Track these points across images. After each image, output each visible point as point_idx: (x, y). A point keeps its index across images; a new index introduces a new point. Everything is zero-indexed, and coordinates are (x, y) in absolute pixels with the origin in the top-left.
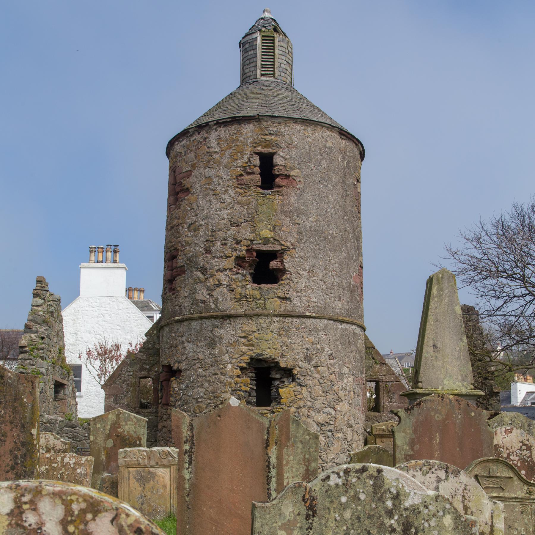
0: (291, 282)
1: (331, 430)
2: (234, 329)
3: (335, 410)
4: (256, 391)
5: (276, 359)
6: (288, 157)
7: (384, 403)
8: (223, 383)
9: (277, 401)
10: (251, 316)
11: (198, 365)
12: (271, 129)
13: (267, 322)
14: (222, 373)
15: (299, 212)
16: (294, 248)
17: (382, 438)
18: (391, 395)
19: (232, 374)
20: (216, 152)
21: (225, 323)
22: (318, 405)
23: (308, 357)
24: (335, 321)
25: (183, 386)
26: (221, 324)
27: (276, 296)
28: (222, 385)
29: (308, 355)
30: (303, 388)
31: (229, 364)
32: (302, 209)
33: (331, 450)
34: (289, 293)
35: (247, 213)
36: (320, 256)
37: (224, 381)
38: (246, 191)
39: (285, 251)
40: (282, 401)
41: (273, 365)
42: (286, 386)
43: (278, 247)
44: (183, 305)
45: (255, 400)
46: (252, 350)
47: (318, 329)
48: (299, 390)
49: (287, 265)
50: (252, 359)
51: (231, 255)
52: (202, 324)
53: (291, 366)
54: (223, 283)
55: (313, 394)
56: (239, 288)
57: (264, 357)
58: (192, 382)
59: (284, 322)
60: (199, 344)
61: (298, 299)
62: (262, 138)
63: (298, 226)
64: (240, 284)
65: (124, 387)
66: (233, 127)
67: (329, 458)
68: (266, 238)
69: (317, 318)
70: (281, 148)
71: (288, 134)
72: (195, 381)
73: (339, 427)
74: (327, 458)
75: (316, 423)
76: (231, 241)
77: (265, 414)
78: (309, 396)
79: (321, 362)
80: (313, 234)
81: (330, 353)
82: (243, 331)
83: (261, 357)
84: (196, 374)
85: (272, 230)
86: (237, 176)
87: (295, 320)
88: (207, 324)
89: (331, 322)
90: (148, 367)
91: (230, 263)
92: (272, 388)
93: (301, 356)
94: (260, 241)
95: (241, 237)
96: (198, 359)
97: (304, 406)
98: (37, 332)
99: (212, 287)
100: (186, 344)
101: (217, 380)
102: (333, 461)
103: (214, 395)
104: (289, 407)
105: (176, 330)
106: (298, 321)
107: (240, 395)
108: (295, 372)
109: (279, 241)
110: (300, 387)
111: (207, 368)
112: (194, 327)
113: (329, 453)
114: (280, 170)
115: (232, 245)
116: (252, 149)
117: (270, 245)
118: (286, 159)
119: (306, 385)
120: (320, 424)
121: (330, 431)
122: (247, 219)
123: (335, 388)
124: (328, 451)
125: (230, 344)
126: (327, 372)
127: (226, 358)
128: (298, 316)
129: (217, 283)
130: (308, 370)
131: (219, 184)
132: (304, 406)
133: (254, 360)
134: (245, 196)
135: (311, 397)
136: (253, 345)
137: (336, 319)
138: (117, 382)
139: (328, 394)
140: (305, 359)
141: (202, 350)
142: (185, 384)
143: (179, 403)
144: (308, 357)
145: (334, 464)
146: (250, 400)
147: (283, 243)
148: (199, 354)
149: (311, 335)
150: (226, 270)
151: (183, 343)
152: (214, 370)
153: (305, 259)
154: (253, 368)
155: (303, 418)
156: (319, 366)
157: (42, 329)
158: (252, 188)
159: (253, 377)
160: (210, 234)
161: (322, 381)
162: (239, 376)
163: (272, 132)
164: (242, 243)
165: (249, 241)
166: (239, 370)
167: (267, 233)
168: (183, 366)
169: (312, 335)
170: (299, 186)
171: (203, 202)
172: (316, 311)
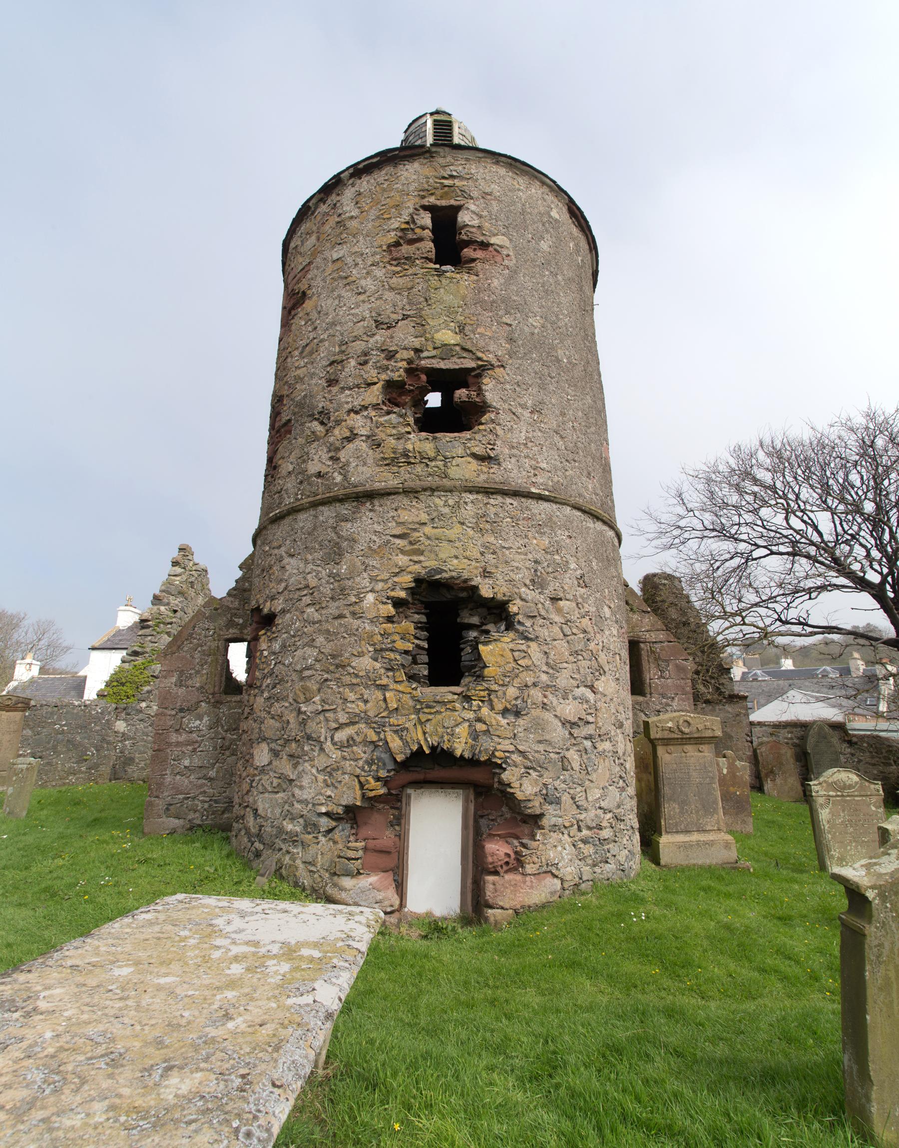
0: (497, 427)
1: (590, 735)
2: (381, 520)
3: (594, 693)
4: (430, 652)
5: (471, 579)
6: (485, 213)
7: (650, 679)
8: (355, 635)
9: (475, 672)
10: (417, 492)
11: (307, 600)
12: (452, 168)
13: (451, 502)
14: (353, 614)
15: (510, 307)
16: (502, 366)
17: (667, 745)
18: (663, 664)
19: (374, 615)
20: (352, 217)
21: (363, 509)
22: (563, 680)
23: (539, 577)
24: (584, 512)
25: (276, 646)
26: (354, 513)
27: (468, 452)
28: (353, 639)
29: (539, 574)
30: (531, 643)
31: (370, 594)
32: (514, 301)
33: (592, 781)
34: (495, 447)
35: (409, 303)
36: (552, 388)
37: (357, 630)
38: (406, 267)
39: (484, 370)
40: (486, 672)
41: (464, 595)
42: (495, 640)
43: (470, 364)
44: (285, 488)
45: (426, 673)
46: (420, 562)
47: (555, 523)
48: (524, 647)
49: (489, 396)
50: (418, 581)
51: (376, 380)
52: (316, 517)
53: (504, 595)
54: (360, 433)
55: (551, 656)
56: (391, 438)
57: (445, 575)
58: (294, 636)
59: (488, 503)
60: (310, 557)
61: (513, 460)
62: (436, 183)
63: (508, 328)
64: (394, 432)
65: (196, 656)
66: (383, 172)
67: (590, 799)
68: (446, 345)
69: (552, 501)
70: (472, 198)
71: (484, 178)
72: (299, 633)
73: (603, 728)
74: (587, 798)
75: (561, 721)
76: (377, 355)
77: (450, 702)
78: (544, 661)
79: (564, 590)
80: (536, 347)
81: (579, 572)
82: (399, 524)
83: (438, 577)
84: (301, 618)
85: (457, 330)
86: (389, 246)
87: (509, 500)
88: (327, 513)
89: (579, 513)
90: (241, 621)
91: (375, 395)
92: (462, 646)
93: (524, 575)
94: (434, 353)
95: (397, 345)
96: (307, 587)
97: (535, 685)
98: (168, 604)
99: (338, 444)
100: (287, 560)
101: (342, 630)
102: (598, 805)
103: (337, 661)
104: (503, 685)
105: (271, 538)
106: (515, 503)
107: (392, 660)
108: (513, 609)
109: (471, 351)
110: (523, 642)
111: (324, 605)
112: (301, 525)
113: (590, 788)
114: (471, 232)
115: (378, 362)
116: (417, 199)
117: (455, 359)
118: (481, 217)
119: (537, 637)
120: (569, 722)
121: (589, 738)
122: (409, 313)
123: (592, 646)
124: (587, 782)
125: (372, 552)
126: (576, 612)
127: (364, 581)
128: (516, 494)
129: (348, 434)
130: (540, 606)
131: (357, 265)
132: (535, 685)
133: (424, 586)
134: (404, 276)
135: (547, 664)
136: (421, 553)
137: (587, 509)
138: (186, 649)
139: (580, 657)
140: (532, 581)
141: (315, 568)
142: (280, 641)
143: (269, 681)
144: (539, 577)
145: (599, 810)
146: (415, 672)
147: (480, 355)
148: (309, 576)
149: (541, 533)
150: (365, 408)
151: (281, 559)
152: (338, 608)
153: (525, 387)
154: (422, 602)
155: (533, 711)
156: (561, 599)
157: (175, 602)
158: (417, 262)
159: (421, 623)
160: (337, 349)
161: (567, 631)
162: (390, 619)
163: (455, 174)
164: (398, 356)
165: (412, 353)
166: (390, 607)
167: (447, 336)
168: (278, 605)
169: (544, 533)
170: (506, 262)
171: (328, 304)
172: (551, 489)
